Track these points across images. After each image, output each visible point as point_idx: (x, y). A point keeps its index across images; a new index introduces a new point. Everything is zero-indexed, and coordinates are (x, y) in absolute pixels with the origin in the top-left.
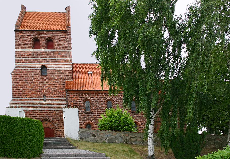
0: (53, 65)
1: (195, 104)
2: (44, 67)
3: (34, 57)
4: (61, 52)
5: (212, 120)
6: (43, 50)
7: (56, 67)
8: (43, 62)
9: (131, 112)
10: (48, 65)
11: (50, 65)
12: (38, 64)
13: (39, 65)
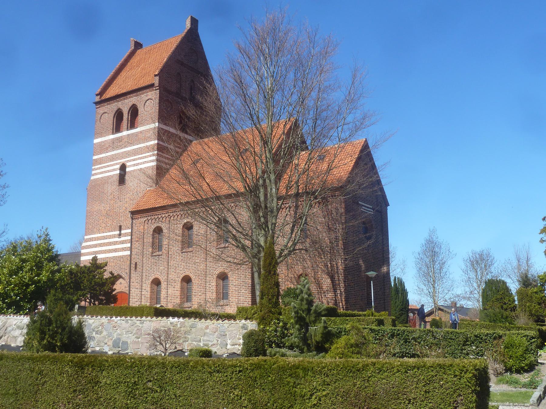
0: (134, 160)
2: (123, 167)
3: (113, 149)
7: (138, 164)
8: (123, 158)
13: (117, 164)
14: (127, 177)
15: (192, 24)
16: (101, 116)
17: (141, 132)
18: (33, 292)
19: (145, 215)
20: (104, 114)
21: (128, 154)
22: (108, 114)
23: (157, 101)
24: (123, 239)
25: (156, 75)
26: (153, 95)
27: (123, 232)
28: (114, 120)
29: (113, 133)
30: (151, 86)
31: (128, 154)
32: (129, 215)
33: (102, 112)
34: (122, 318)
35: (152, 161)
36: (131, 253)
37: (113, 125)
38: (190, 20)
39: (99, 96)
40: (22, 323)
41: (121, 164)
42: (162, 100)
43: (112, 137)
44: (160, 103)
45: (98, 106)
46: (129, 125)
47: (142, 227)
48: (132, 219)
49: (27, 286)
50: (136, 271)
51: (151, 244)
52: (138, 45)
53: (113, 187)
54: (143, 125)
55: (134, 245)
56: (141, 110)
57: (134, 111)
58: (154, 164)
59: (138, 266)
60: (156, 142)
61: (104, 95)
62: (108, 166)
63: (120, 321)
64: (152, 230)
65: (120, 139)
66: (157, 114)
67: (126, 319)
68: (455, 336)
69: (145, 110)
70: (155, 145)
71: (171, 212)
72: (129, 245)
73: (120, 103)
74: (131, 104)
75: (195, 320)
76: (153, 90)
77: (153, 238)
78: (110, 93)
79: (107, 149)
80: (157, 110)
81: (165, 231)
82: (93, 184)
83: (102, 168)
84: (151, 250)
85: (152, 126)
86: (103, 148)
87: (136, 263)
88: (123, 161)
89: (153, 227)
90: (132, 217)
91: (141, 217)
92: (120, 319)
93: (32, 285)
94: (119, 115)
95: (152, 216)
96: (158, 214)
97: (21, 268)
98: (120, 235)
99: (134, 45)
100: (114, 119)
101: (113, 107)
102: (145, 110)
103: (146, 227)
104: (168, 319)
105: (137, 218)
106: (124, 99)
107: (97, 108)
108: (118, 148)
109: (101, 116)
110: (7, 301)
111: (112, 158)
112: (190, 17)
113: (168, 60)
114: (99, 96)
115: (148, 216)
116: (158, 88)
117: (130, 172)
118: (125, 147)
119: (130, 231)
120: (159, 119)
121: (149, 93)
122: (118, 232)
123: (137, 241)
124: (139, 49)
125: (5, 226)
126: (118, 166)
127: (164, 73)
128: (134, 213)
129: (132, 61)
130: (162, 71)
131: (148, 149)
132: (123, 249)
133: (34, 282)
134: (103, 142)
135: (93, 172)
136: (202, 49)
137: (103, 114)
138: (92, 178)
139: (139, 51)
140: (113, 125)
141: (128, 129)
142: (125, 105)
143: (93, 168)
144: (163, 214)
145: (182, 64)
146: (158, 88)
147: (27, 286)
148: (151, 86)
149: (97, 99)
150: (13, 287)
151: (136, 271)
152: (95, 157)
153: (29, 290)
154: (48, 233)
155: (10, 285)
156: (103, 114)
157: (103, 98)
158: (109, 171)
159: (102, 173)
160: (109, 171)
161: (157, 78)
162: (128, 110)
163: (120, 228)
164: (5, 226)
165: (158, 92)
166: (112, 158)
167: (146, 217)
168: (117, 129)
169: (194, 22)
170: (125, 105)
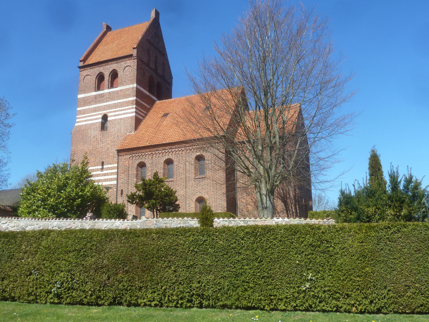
0: (115, 112)
1: (385, 184)
2: (105, 118)
3: (96, 103)
4: (125, 90)
5: (387, 295)
6: (106, 91)
7: (117, 115)
8: (104, 110)
9: (195, 179)
10: (109, 112)
11: (111, 112)
12: (97, 115)
13: (99, 114)
14: (108, 124)
15: (156, 15)
16: (85, 77)
17: (121, 91)
18: (78, 206)
19: (129, 153)
20: (87, 76)
21: (110, 107)
22: (91, 76)
23: (135, 67)
24: (105, 172)
25: (134, 48)
26: (133, 63)
27: (105, 167)
28: (96, 81)
29: (95, 91)
30: (130, 56)
31: (110, 107)
32: (116, 153)
33: (86, 74)
34: (224, 220)
35: (132, 113)
36: (117, 182)
37: (96, 85)
38: (154, 12)
39: (83, 62)
40: (114, 225)
41: (103, 114)
42: (139, 69)
43: (94, 93)
44: (137, 69)
45: (82, 70)
46: (110, 85)
47: (127, 162)
48: (118, 156)
49: (74, 200)
50: (122, 197)
51: (135, 175)
52: (109, 29)
53: (96, 132)
54: (122, 85)
55: (120, 176)
56: (120, 74)
57: (114, 75)
58: (134, 114)
59: (124, 192)
60: (135, 98)
61: (87, 62)
62: (91, 116)
63: (222, 222)
64: (136, 165)
65: (102, 96)
66: (135, 77)
67: (229, 220)
68: (411, 241)
69: (124, 74)
70: (133, 101)
71: (153, 151)
72: (115, 176)
73: (101, 68)
74: (111, 69)
75: (300, 220)
76: (132, 59)
77: (137, 171)
78: (92, 60)
79: (90, 103)
80: (136, 75)
81: (148, 165)
82: (77, 129)
83: (85, 117)
84: (135, 180)
85: (131, 86)
86: (86, 102)
87: (122, 190)
88: (105, 112)
89: (137, 162)
90: (118, 155)
91: (126, 155)
92: (223, 220)
93: (78, 199)
94: (101, 78)
95: (136, 153)
96: (142, 153)
97: (65, 185)
98: (102, 169)
99: (106, 28)
100: (96, 80)
101: (96, 70)
102: (124, 74)
103: (130, 162)
104: (273, 219)
105: (122, 155)
106: (106, 65)
107: (80, 71)
108: (100, 102)
109: (85, 77)
110: (57, 212)
111: (95, 110)
112: (154, 10)
113: (142, 38)
114: (83, 62)
115: (133, 154)
116: (136, 58)
117: (111, 120)
118: (107, 101)
119: (116, 165)
120: (137, 81)
121: (128, 62)
122: (101, 167)
123: (123, 173)
124: (109, 31)
125: (9, 158)
126: (101, 116)
127: (140, 47)
128: (119, 151)
129: (105, 39)
130: (138, 45)
131: (131, 103)
132: (111, 180)
133: (80, 197)
134: (87, 97)
135: (77, 120)
136: (162, 34)
137: (86, 76)
138: (76, 125)
139: (109, 33)
140: (96, 85)
141: (108, 88)
142: (106, 70)
143: (77, 117)
144: (148, 152)
145: (150, 43)
146: (136, 58)
147: (74, 200)
148: (130, 56)
149: (81, 64)
150: (62, 200)
151: (122, 197)
152: (78, 109)
153: (75, 203)
154: (87, 157)
155: (59, 199)
156: (86, 76)
157: (87, 63)
158: (91, 120)
159: (86, 121)
160: (91, 120)
161: (136, 50)
162: (109, 73)
163: (103, 164)
164: (9, 158)
165: (136, 61)
166: (95, 110)
167: (131, 154)
168: (98, 88)
169: (157, 13)
170: (106, 70)
